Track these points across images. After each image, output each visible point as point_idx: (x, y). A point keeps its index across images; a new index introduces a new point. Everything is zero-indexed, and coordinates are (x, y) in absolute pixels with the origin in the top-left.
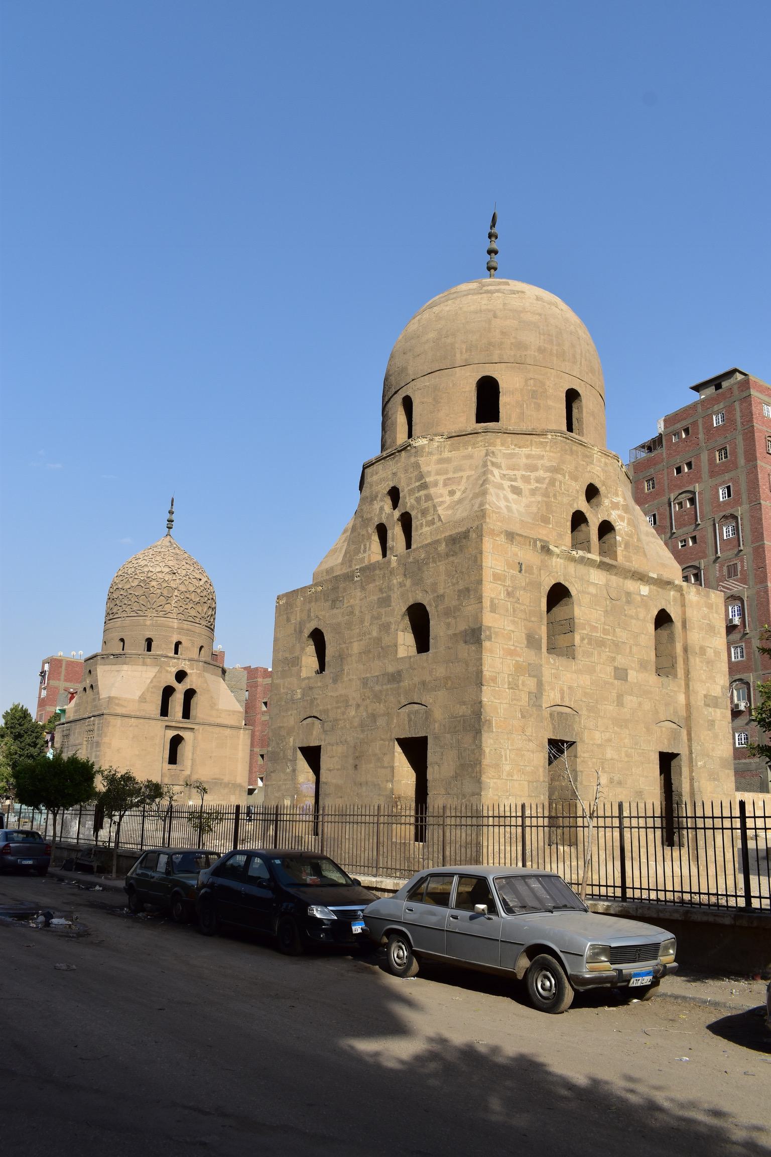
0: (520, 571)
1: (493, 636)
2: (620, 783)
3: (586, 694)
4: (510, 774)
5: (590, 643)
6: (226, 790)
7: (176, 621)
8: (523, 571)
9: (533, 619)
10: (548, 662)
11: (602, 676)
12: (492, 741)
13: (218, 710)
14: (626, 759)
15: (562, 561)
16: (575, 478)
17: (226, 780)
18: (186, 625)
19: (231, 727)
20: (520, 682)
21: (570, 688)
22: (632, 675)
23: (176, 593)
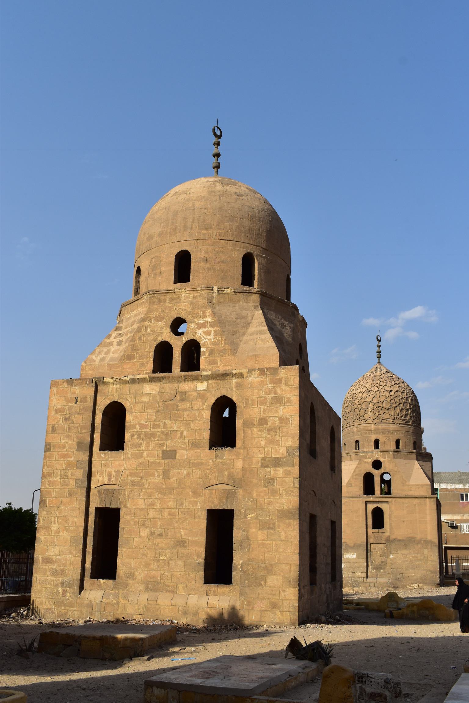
0: (76, 403)
1: (52, 448)
2: (161, 535)
3: (131, 474)
4: (57, 532)
5: (139, 437)
6: (419, 546)
7: (373, 425)
8: (79, 402)
9: (83, 431)
10: (100, 457)
12: (45, 513)
13: (409, 485)
15: (118, 386)
16: (159, 319)
17: (418, 537)
18: (380, 427)
19: (418, 497)
20: (70, 473)
21: (117, 471)
22: (181, 454)
23: (371, 405)
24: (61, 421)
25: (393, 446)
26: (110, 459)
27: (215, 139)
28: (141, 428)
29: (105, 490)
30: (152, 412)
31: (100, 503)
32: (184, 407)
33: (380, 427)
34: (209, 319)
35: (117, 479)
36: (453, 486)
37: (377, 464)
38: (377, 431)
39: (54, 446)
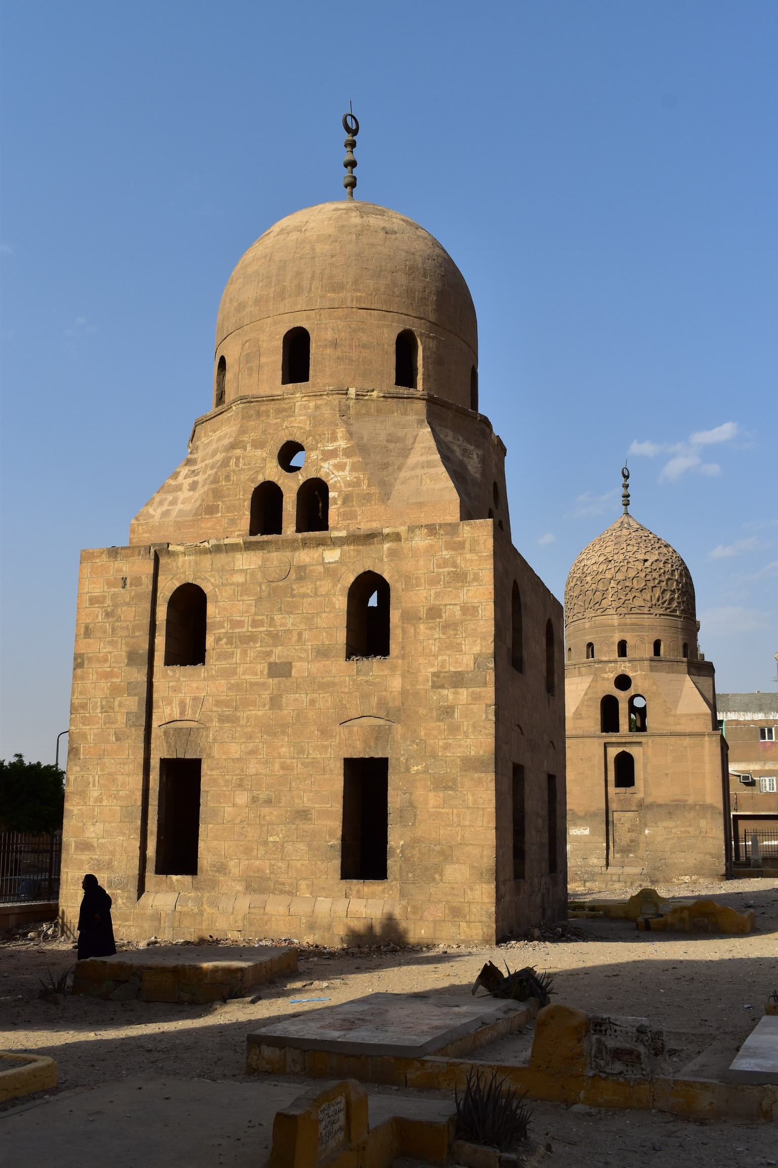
1: (86, 662)
2: (269, 802)
3: (218, 703)
4: (99, 800)
5: (230, 642)
6: (693, 814)
7: (616, 617)
8: (128, 585)
9: (137, 634)
11: (247, 677)
14: (282, 772)
15: (192, 558)
16: (258, 444)
17: (691, 801)
18: (629, 620)
19: (691, 735)
20: (116, 703)
21: (195, 699)
22: (299, 669)
24: (100, 618)
25: (649, 652)
26: (182, 679)
27: (348, 137)
28: (232, 627)
29: (175, 730)
30: (249, 600)
31: (168, 751)
32: (302, 590)
33: (628, 621)
34: (342, 444)
35: (194, 712)
36: (749, 717)
37: (623, 682)
38: (622, 627)
39: (90, 659)
